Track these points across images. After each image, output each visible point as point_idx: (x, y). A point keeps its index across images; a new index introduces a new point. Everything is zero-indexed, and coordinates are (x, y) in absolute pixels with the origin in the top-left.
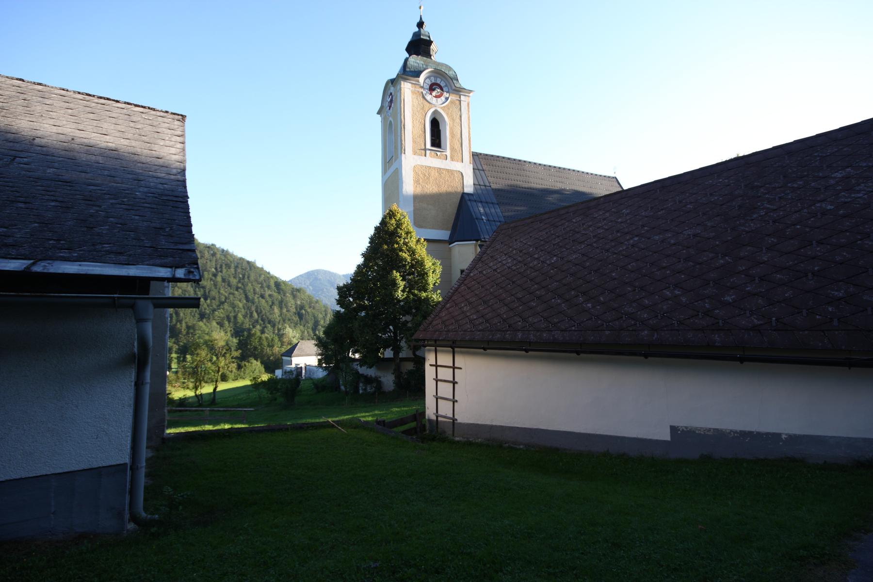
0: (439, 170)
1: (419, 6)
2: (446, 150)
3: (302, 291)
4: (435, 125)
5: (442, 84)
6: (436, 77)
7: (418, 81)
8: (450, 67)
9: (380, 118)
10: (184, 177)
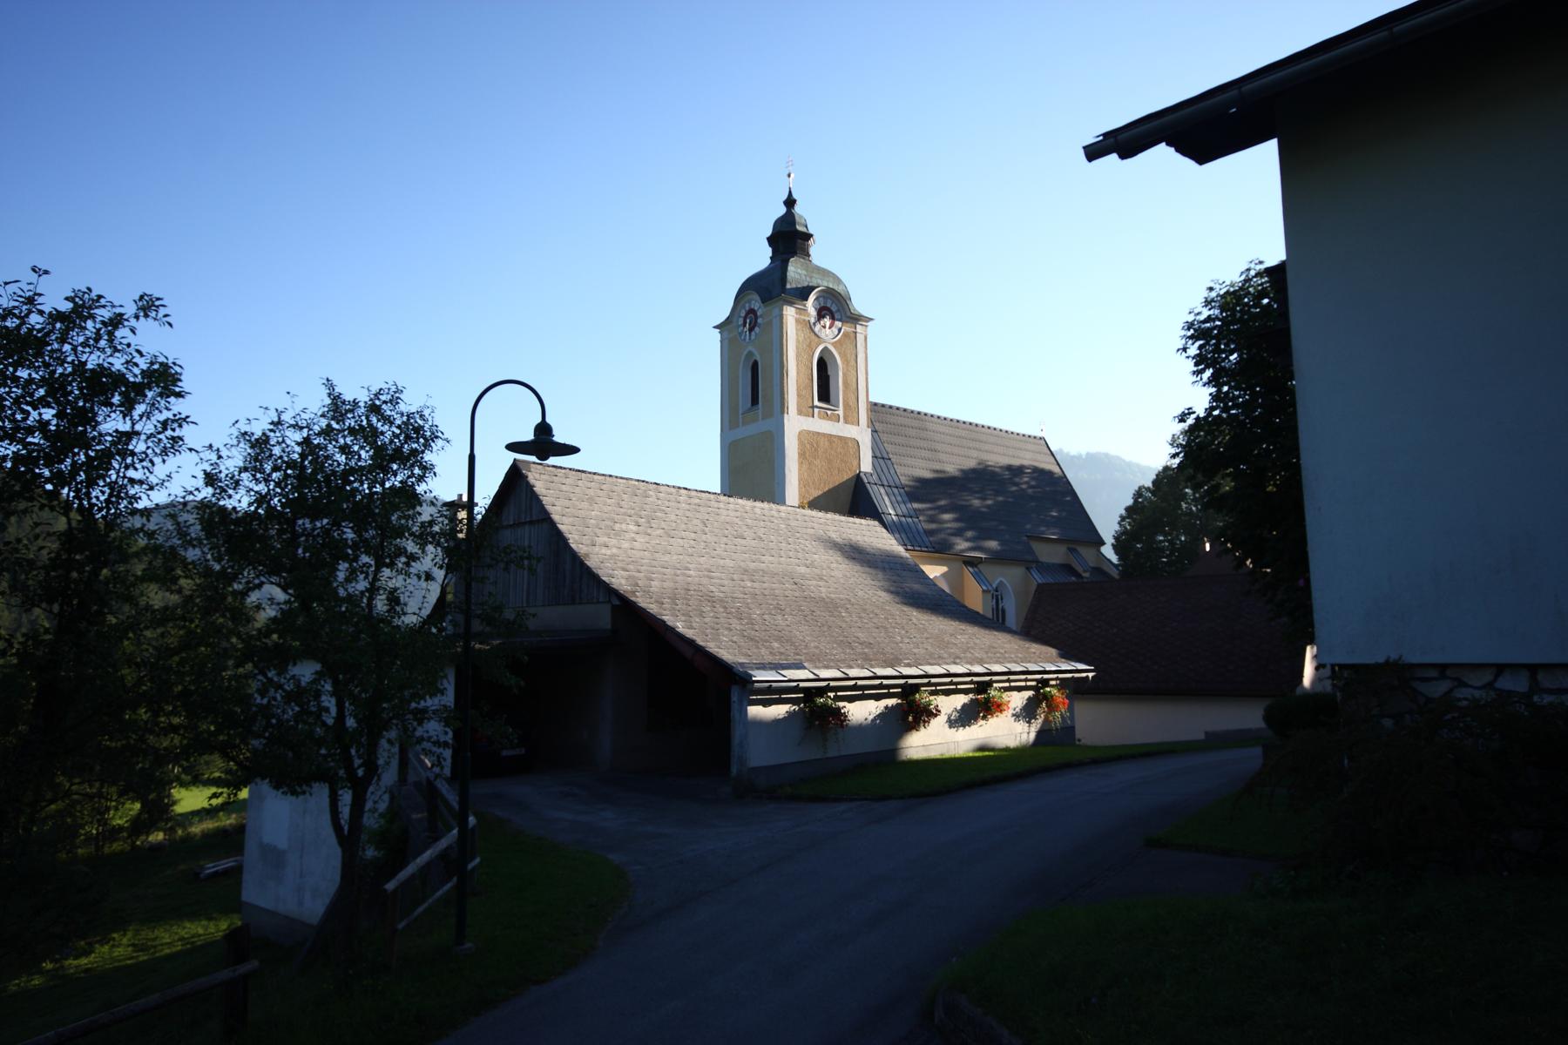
0: (830, 437)
1: (787, 173)
2: (838, 407)
5: (834, 309)
7: (805, 306)
8: (841, 280)
9: (719, 335)
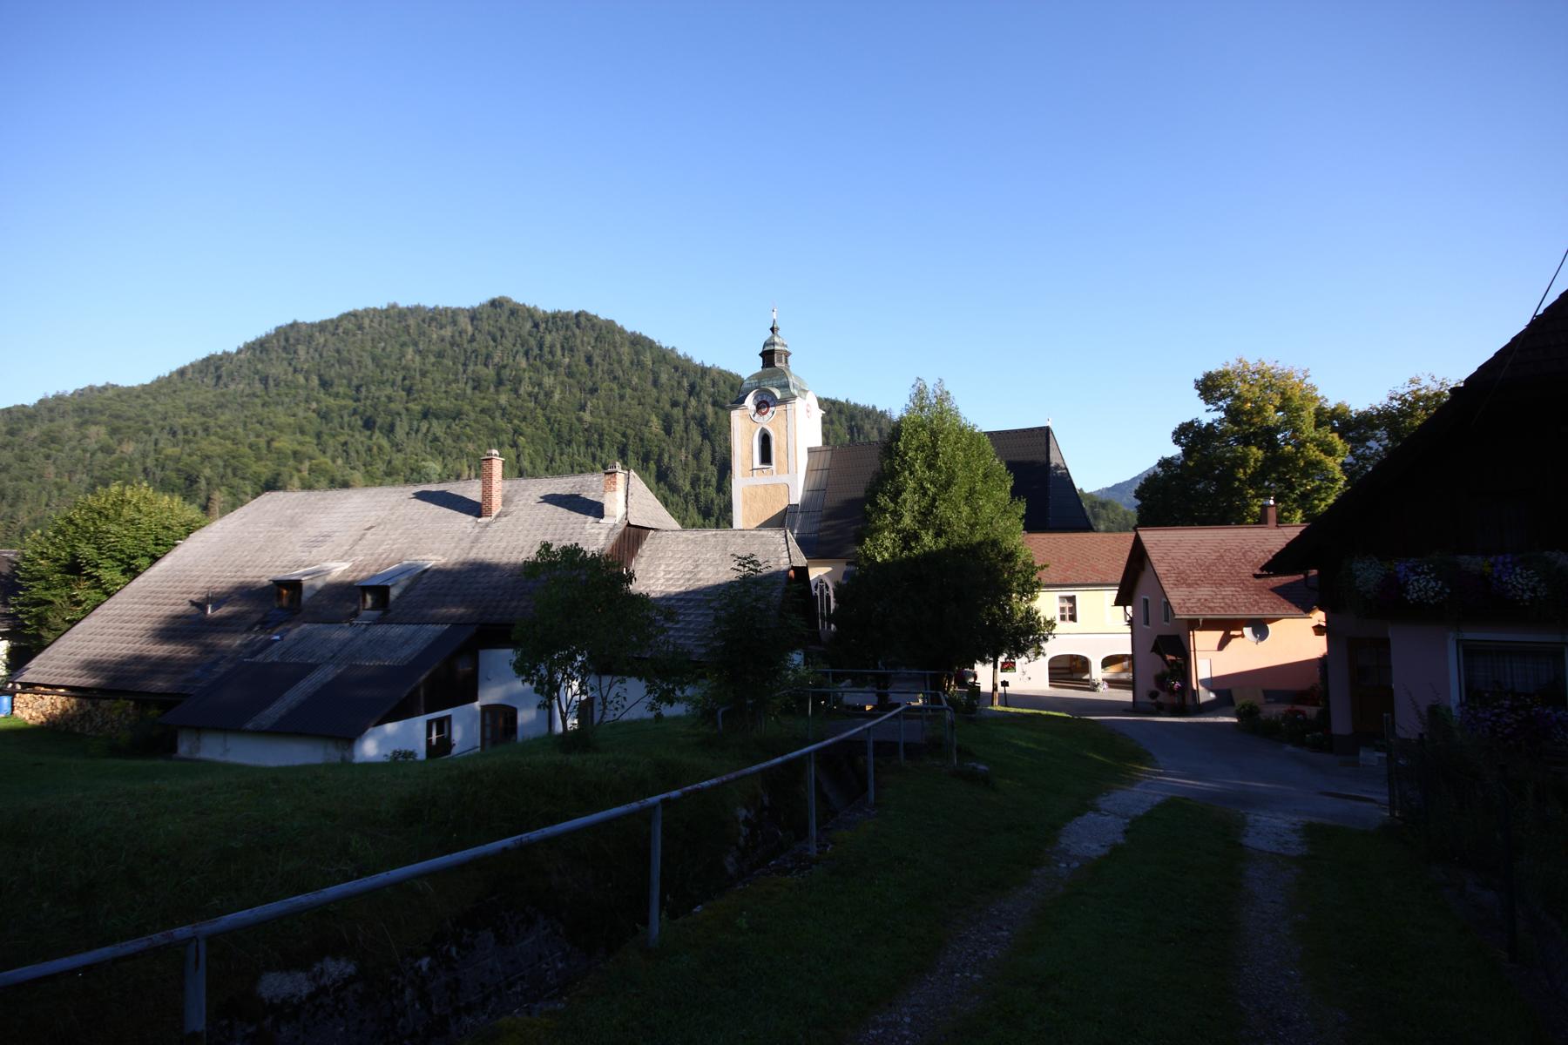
3: (1109, 506)
4: (765, 440)
6: (762, 395)
10: (812, 756)
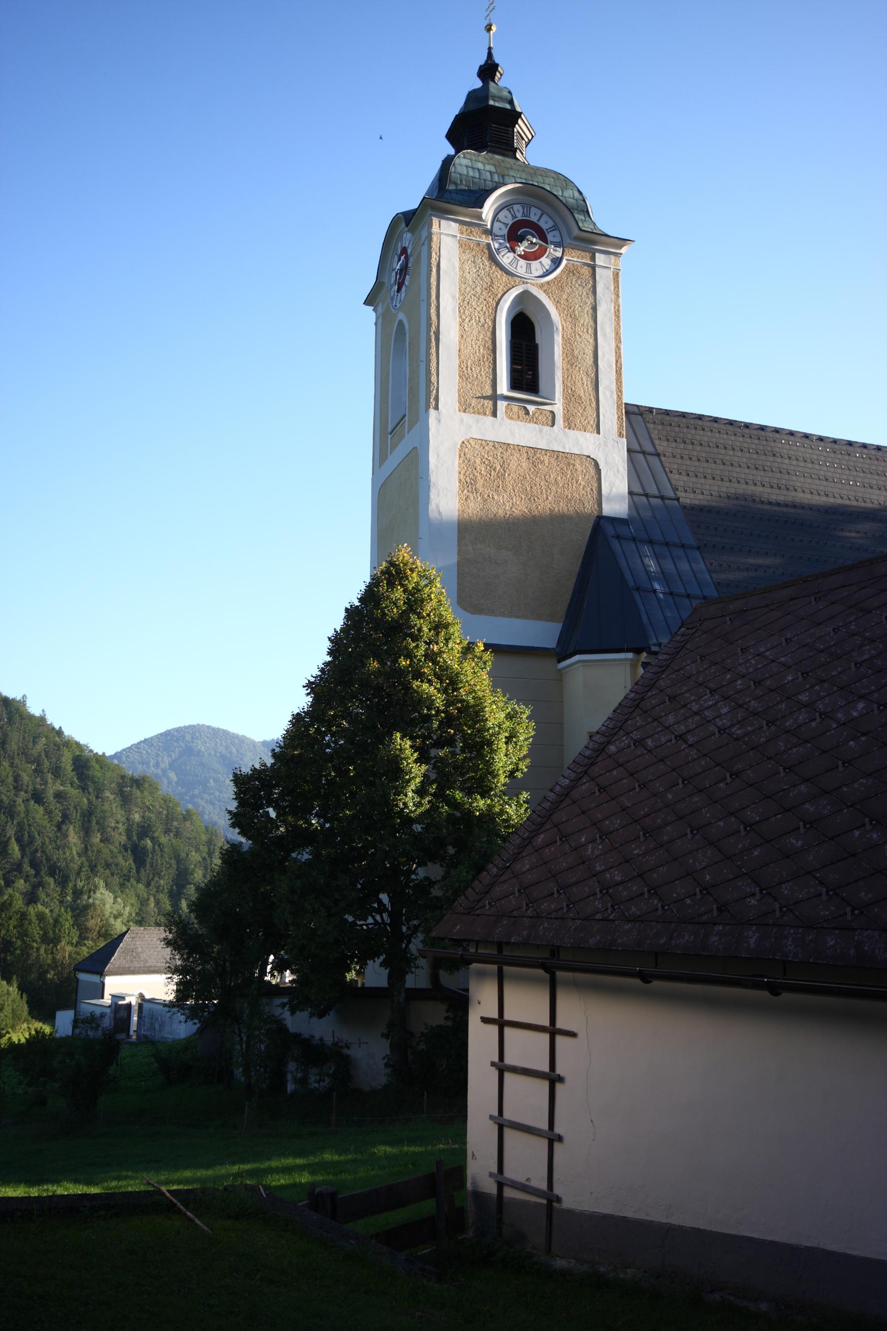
5: (545, 224)
